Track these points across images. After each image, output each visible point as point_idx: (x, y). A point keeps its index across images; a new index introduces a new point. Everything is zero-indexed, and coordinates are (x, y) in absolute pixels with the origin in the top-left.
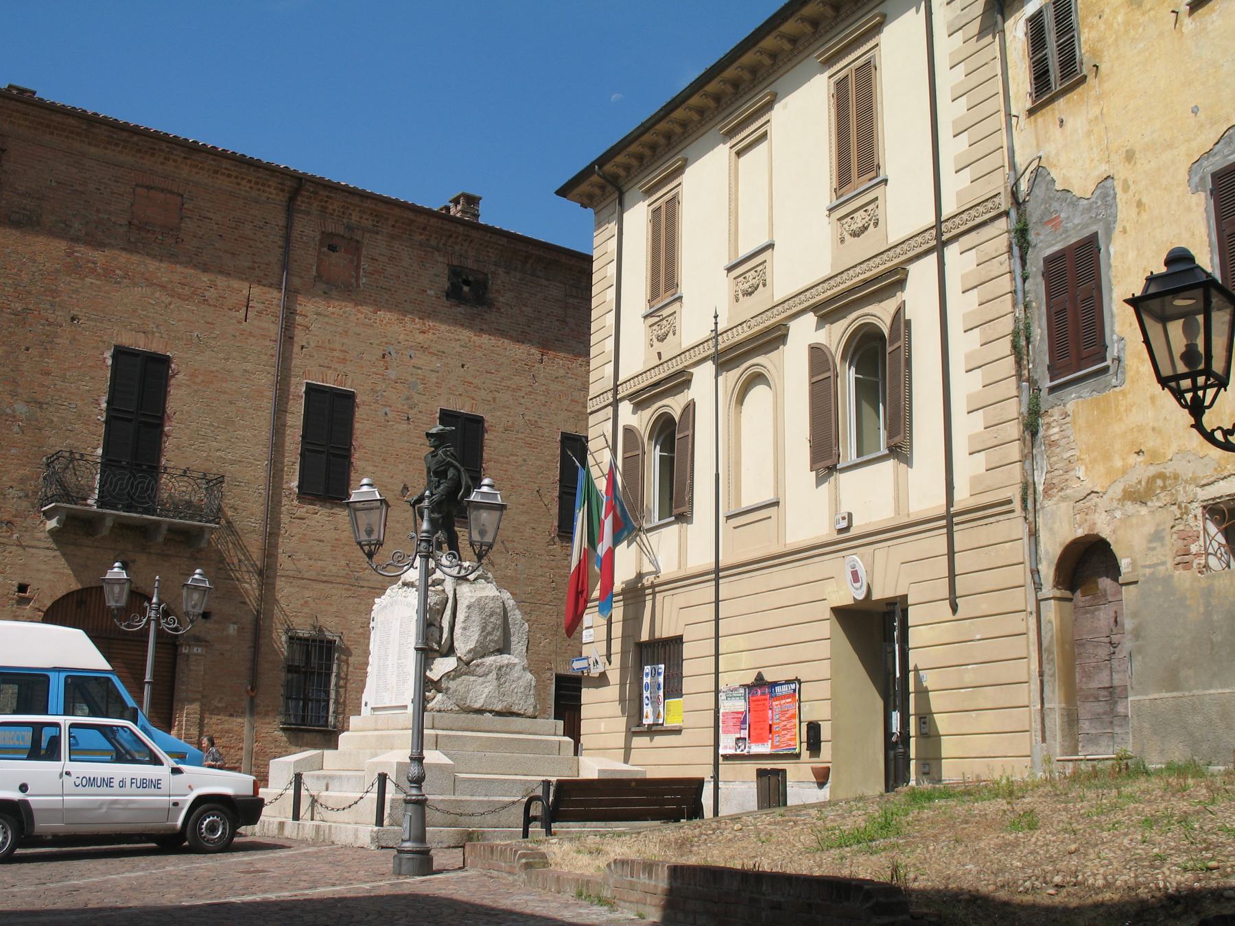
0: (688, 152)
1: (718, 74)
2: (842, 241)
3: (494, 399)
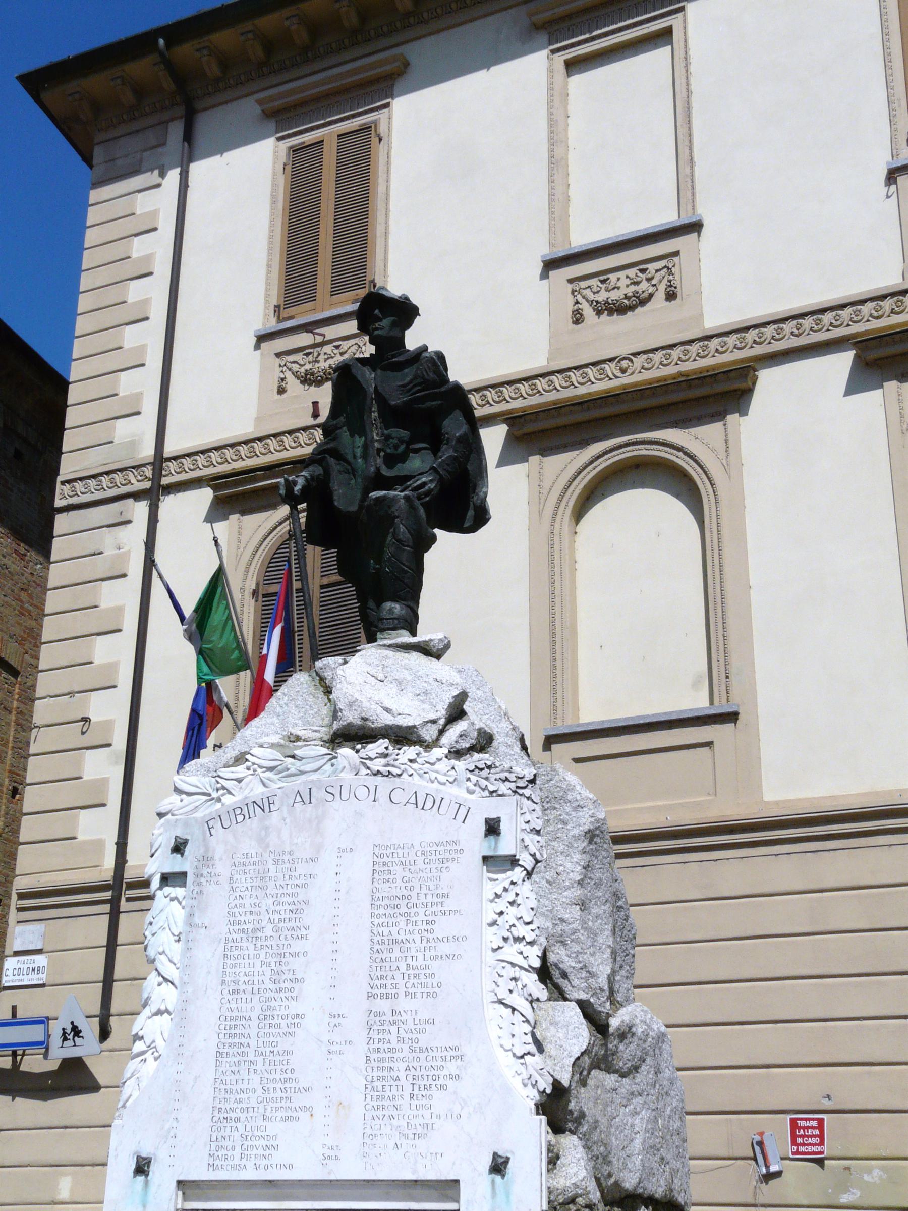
0: (419, 52)
2: (281, 391)
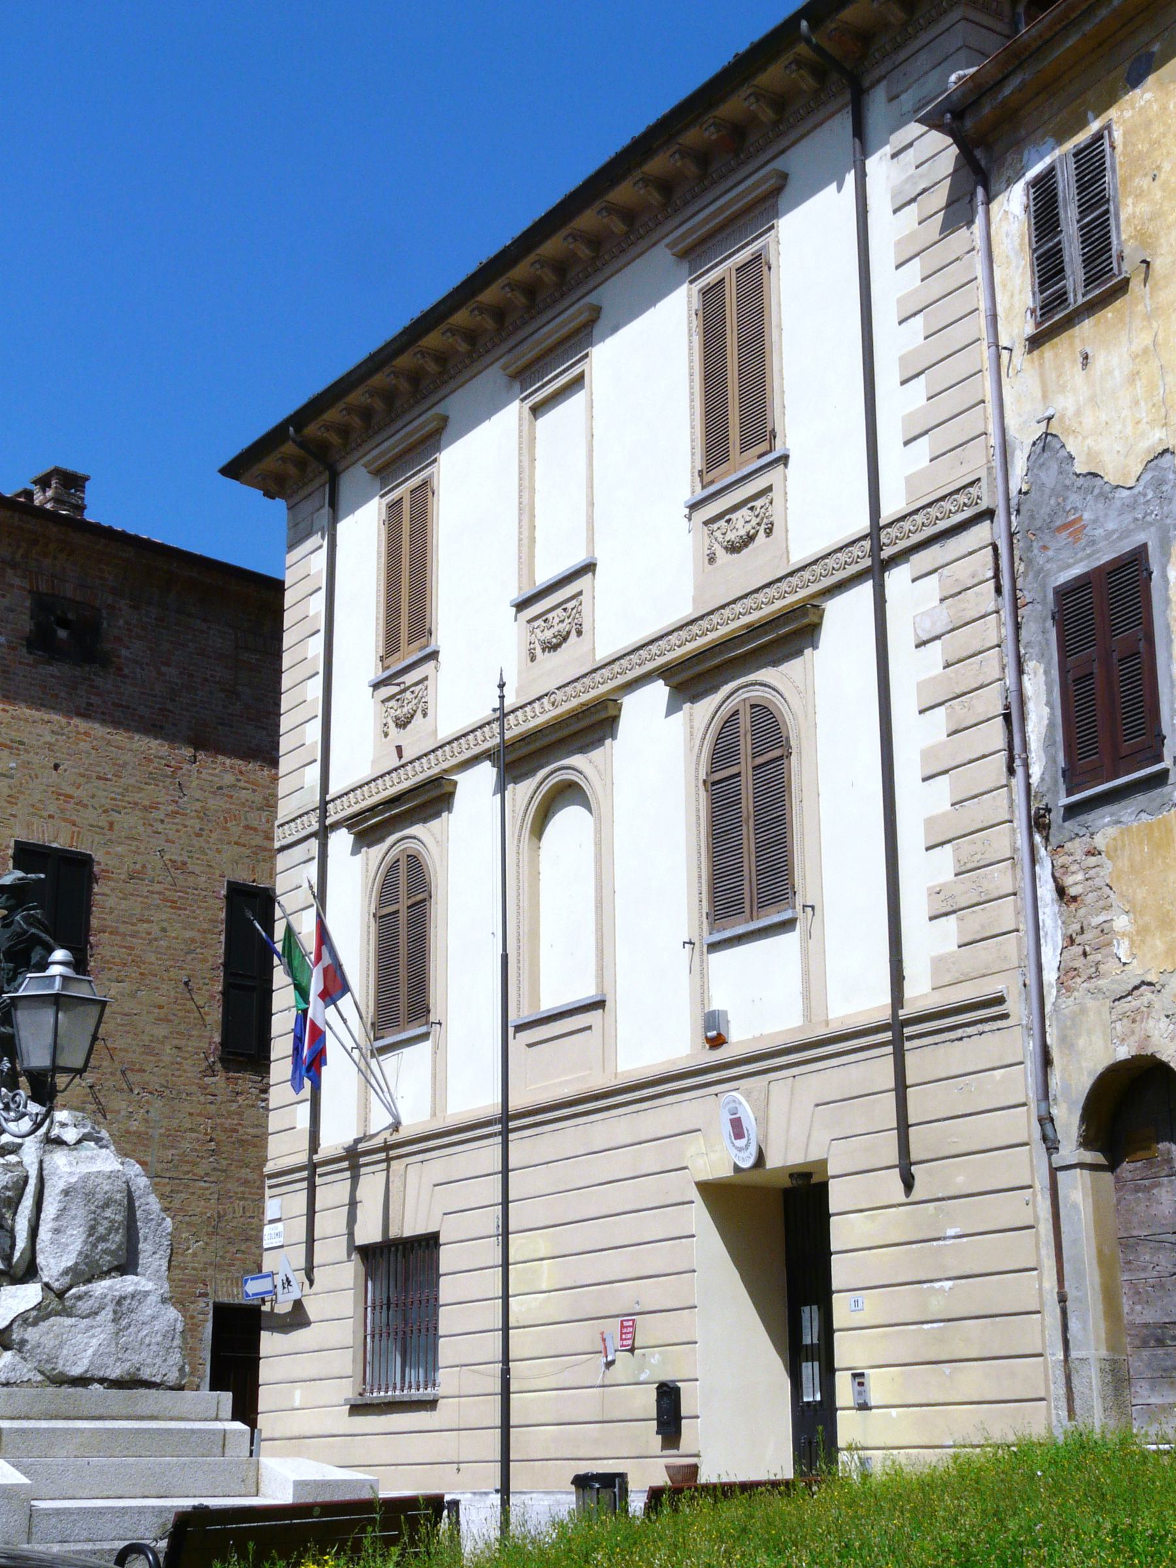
1: (501, 274)
2: (712, 559)
3: (111, 824)
